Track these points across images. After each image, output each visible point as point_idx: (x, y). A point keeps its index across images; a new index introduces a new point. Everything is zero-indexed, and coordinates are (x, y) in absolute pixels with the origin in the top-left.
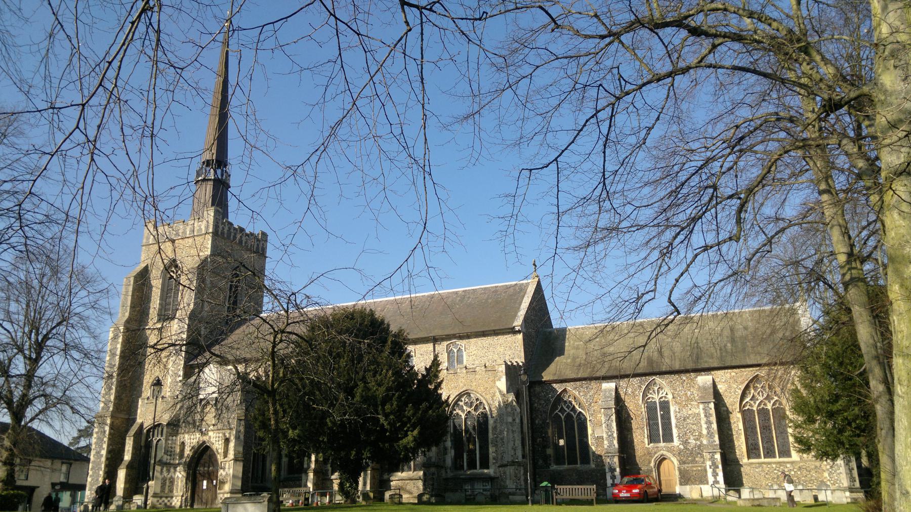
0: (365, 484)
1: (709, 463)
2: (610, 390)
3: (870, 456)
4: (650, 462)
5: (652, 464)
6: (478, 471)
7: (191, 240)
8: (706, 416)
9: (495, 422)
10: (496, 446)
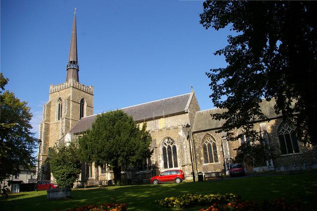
6: (174, 168)
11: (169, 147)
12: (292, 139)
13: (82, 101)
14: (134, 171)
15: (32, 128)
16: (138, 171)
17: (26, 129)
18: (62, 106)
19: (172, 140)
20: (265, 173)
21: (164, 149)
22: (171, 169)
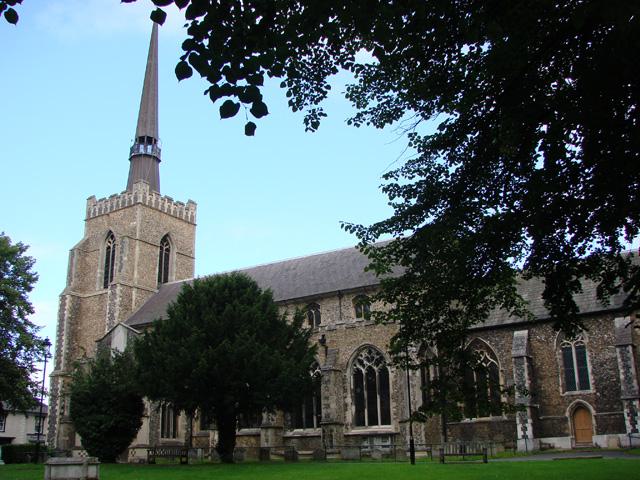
0: (524, 429)
1: (626, 411)
2: (522, 338)
3: (162, 466)
4: (564, 412)
5: (567, 414)
7: (122, 212)
8: (623, 360)
9: (395, 377)
10: (396, 401)
11: (370, 370)
12: (578, 365)
13: (165, 239)
14: (280, 428)
15: (32, 313)
16: (292, 428)
17: (21, 314)
18: (114, 251)
19: (378, 353)
20: (622, 450)
21: (358, 374)
22: (374, 429)
